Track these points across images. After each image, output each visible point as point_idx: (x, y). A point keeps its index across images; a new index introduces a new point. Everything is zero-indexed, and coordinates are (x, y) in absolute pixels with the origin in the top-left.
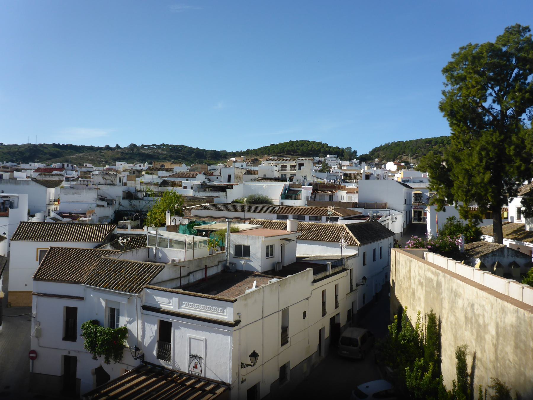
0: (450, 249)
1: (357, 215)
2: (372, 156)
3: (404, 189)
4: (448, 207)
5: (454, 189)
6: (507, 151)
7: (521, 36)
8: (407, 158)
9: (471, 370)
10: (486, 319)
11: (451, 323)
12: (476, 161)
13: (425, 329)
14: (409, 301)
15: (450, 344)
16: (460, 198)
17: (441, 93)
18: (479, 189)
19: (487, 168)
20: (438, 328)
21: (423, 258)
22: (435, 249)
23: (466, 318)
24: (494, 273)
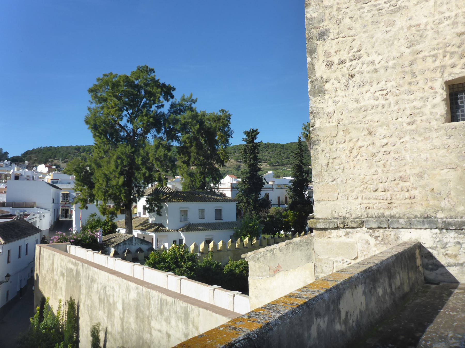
0: (90, 241)
1: (4, 214)
2: (23, 159)
3: (53, 189)
4: (90, 205)
5: (95, 190)
6: (136, 161)
7: (148, 74)
8: (58, 162)
9: (103, 344)
10: (115, 298)
11: (88, 306)
12: (113, 166)
13: (66, 315)
14: (52, 291)
15: (87, 324)
16: (99, 197)
17: (87, 108)
18: (115, 190)
19: (121, 173)
20: (76, 312)
21: (66, 251)
22: (78, 243)
23: (100, 299)
24: (124, 259)
